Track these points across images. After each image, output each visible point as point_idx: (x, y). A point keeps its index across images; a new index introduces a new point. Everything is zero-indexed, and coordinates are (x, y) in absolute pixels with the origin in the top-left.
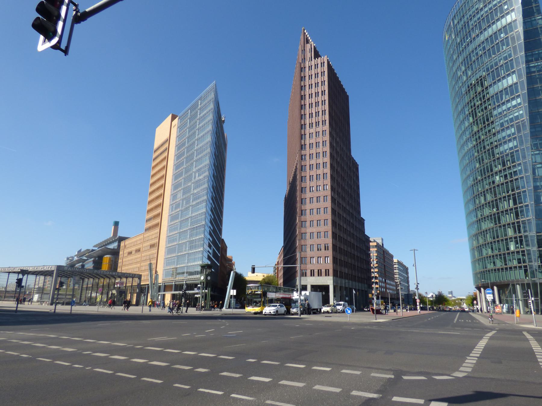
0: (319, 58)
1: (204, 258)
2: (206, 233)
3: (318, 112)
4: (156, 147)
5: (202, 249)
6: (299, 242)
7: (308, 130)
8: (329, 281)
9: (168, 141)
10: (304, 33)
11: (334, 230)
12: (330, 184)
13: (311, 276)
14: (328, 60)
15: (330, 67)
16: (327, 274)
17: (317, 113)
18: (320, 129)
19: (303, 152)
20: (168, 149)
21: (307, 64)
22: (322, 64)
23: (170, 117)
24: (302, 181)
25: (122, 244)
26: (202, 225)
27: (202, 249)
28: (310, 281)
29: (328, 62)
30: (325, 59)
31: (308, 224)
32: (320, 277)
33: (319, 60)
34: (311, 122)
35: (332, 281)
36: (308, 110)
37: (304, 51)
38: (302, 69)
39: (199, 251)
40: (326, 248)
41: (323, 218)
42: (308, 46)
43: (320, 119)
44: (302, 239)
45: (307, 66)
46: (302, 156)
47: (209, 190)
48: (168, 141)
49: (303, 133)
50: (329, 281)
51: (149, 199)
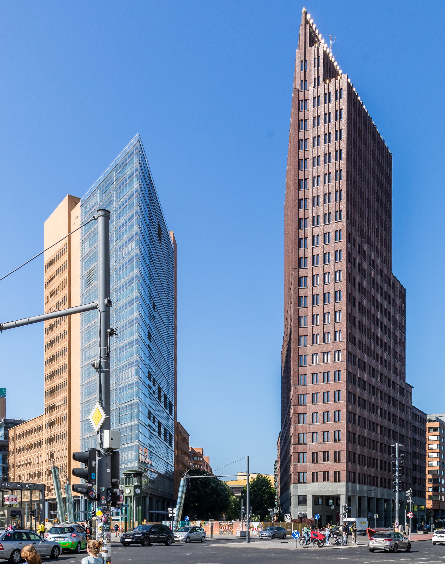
0: (333, 80)
1: (141, 415)
2: (142, 417)
3: (329, 194)
4: (48, 257)
5: (136, 443)
6: (295, 428)
7: (310, 231)
8: (340, 488)
9: (67, 248)
10: (307, 22)
11: (349, 331)
12: (345, 330)
13: (313, 481)
14: (348, 84)
15: (352, 98)
16: (337, 478)
17: (327, 217)
18: (330, 228)
19: (302, 273)
20: (67, 265)
21: (310, 93)
22: (338, 92)
23: (65, 201)
24: (299, 285)
25: (11, 433)
26: (134, 404)
27: (136, 443)
28: (310, 489)
29: (349, 87)
30: (343, 80)
31: (309, 398)
32: (326, 484)
33: (332, 85)
34: (315, 215)
35: (344, 490)
36: (311, 190)
37: (304, 62)
38: (301, 104)
39: (133, 446)
40: (337, 458)
41: (333, 389)
42: (312, 51)
43: (332, 207)
44: (299, 422)
45: (310, 256)
46: (299, 317)
47: (141, 344)
48: (67, 248)
49: (301, 235)
50: (340, 488)
51: (48, 291)
